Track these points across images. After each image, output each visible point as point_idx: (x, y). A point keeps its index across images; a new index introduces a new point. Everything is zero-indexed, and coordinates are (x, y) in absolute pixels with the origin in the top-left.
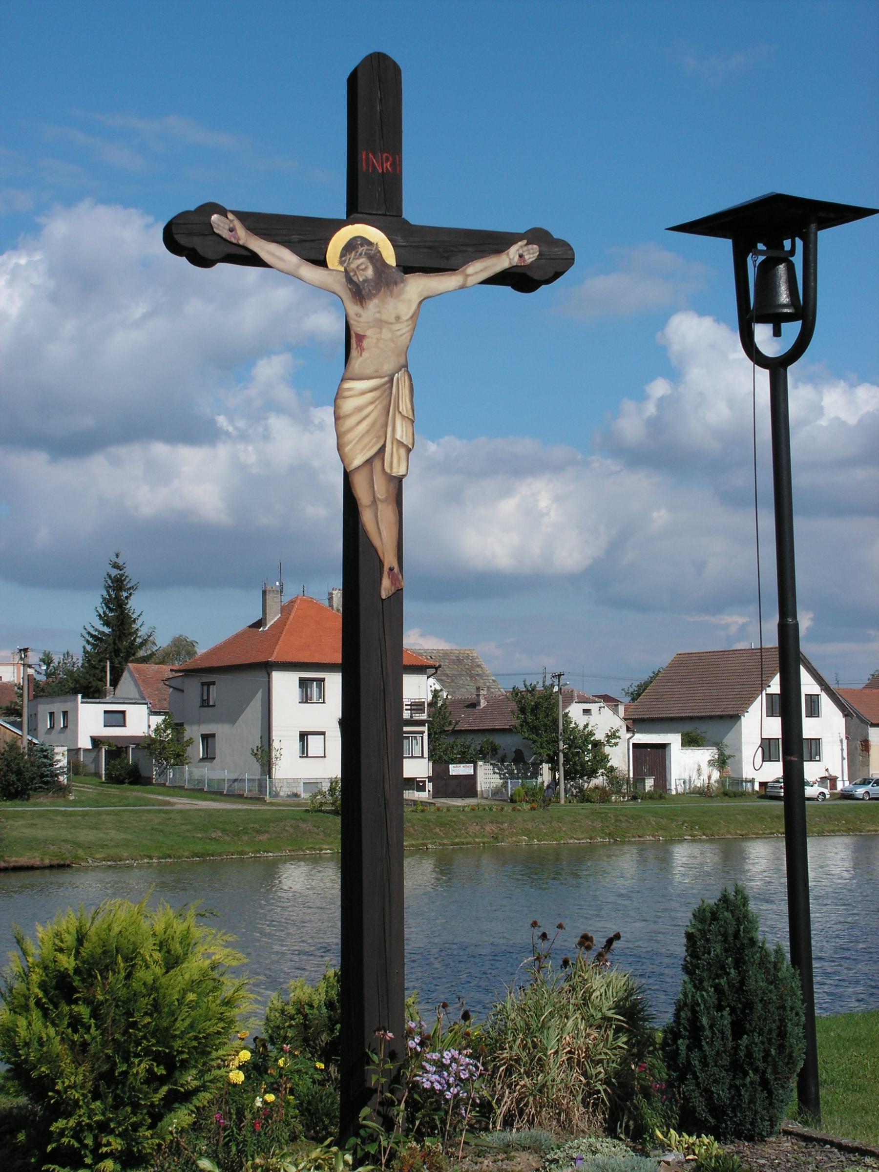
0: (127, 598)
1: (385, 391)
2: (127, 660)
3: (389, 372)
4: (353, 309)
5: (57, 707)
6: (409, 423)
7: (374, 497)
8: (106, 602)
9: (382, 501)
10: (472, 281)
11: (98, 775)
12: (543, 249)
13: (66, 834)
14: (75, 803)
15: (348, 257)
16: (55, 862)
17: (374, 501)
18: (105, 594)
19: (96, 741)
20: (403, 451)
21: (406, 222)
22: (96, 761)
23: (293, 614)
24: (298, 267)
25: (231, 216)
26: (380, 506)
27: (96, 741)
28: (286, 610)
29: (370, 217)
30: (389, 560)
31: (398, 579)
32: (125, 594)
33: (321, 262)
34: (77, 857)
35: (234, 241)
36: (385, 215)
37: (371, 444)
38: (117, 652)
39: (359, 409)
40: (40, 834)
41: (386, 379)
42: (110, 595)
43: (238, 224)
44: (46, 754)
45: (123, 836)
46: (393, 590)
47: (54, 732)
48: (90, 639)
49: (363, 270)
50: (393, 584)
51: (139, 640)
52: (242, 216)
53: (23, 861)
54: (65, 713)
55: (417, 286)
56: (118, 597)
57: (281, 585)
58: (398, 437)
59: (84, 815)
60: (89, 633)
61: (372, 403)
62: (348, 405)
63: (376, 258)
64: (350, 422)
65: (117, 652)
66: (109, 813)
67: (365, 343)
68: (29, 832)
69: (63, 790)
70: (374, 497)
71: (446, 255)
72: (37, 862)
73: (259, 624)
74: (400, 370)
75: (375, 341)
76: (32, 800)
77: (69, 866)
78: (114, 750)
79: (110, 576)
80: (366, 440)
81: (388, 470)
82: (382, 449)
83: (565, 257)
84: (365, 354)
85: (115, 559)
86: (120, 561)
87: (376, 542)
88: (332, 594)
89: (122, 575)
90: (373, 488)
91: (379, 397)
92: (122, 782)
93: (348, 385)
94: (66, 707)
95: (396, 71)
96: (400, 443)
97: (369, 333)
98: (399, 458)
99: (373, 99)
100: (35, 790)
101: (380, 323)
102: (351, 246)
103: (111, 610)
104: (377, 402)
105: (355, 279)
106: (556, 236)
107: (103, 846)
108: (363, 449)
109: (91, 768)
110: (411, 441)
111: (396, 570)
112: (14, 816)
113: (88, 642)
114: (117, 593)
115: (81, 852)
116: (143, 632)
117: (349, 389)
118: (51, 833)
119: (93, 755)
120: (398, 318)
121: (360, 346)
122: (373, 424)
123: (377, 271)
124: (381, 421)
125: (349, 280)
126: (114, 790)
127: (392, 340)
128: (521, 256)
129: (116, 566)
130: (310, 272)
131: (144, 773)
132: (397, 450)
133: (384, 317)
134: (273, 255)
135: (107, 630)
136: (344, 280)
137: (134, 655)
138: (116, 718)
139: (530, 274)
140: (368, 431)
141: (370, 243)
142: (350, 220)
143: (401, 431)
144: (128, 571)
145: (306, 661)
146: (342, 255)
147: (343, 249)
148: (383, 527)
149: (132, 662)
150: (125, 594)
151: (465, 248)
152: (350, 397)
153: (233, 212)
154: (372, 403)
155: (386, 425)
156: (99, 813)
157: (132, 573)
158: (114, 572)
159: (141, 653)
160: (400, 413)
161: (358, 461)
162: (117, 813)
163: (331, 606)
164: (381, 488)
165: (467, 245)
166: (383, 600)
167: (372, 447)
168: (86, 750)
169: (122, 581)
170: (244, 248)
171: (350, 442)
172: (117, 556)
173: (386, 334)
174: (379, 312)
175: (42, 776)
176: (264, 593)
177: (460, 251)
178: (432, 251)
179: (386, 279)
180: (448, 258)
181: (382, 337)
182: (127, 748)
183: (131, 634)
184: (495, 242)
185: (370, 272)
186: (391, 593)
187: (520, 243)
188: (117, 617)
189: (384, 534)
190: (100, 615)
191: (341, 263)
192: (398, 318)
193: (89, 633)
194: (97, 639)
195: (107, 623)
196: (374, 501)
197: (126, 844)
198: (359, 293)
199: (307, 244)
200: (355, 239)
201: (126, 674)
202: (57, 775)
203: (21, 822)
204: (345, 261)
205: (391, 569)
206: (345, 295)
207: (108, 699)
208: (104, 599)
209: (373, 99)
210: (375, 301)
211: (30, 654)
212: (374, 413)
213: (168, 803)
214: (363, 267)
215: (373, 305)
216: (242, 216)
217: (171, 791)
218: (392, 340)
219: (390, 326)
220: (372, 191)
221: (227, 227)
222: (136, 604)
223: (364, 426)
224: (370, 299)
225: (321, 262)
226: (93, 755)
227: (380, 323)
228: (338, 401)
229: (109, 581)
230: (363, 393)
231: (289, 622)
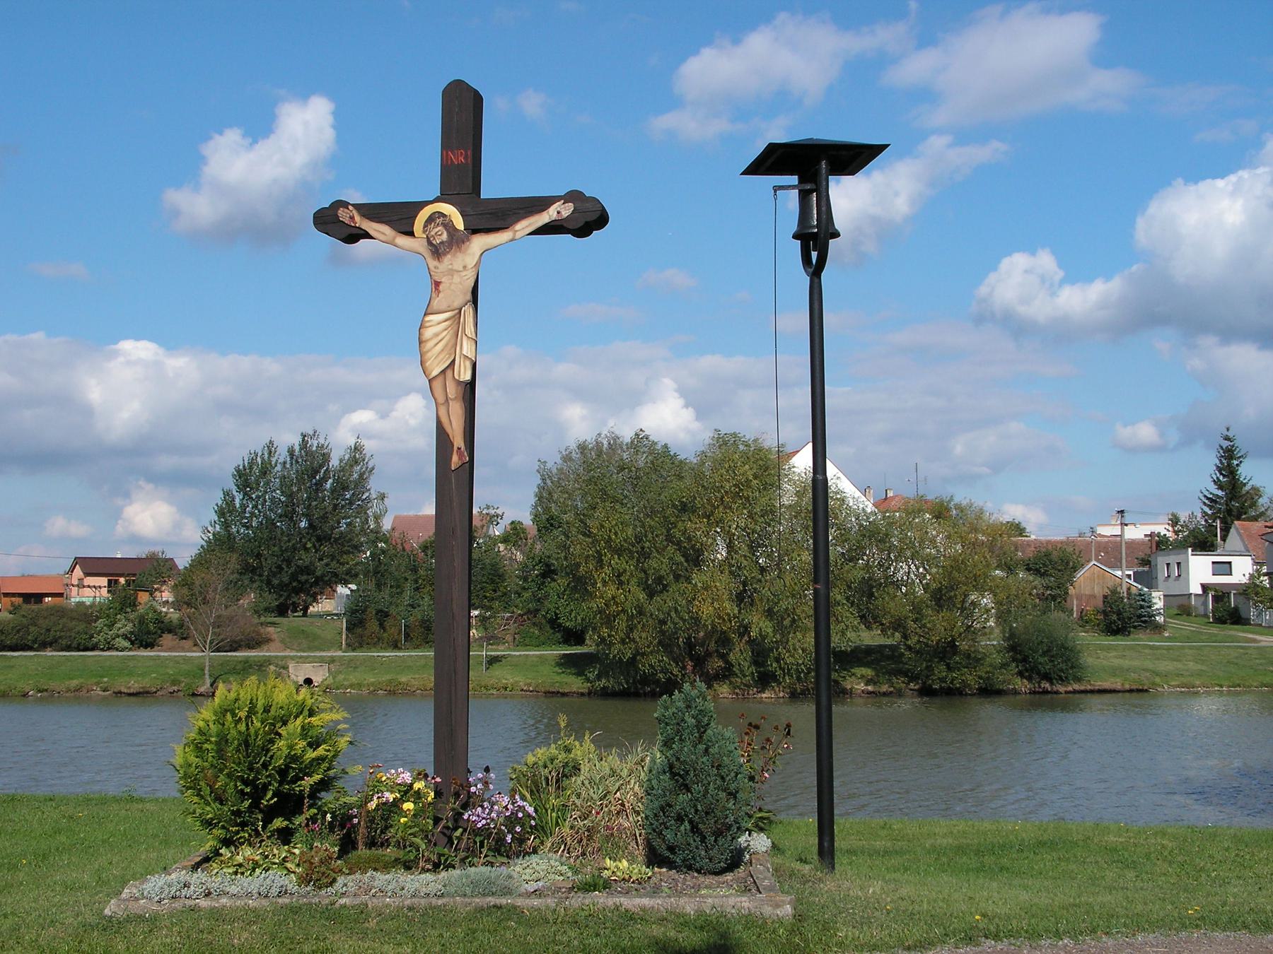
4: (432, 263)
5: (1173, 559)
8: (1220, 470)
10: (518, 235)
11: (1206, 616)
13: (1149, 664)
14: (1169, 639)
16: (1134, 687)
19: (1205, 587)
22: (1205, 604)
27: (1205, 587)
32: (1235, 462)
33: (411, 234)
34: (1154, 684)
39: (437, 335)
40: (1126, 663)
43: (355, 212)
44: (1146, 601)
45: (1200, 667)
47: (1171, 580)
52: (358, 207)
53: (1106, 685)
54: (1179, 564)
55: (479, 243)
56: (1229, 465)
59: (1169, 648)
62: (428, 333)
63: (449, 226)
64: (429, 345)
65: (1229, 512)
66: (1190, 648)
67: (441, 288)
68: (1117, 662)
69: (1158, 628)
72: (1119, 687)
76: (1132, 636)
77: (1146, 691)
78: (1219, 594)
82: (454, 361)
86: (1230, 434)
92: (1224, 622)
93: (427, 318)
94: (1179, 558)
99: (463, 113)
100: (1135, 627)
101: (451, 272)
102: (431, 219)
107: (1178, 675)
109: (1201, 610)
112: (1109, 648)
115: (1158, 680)
118: (1136, 663)
119: (1202, 599)
120: (465, 267)
122: (446, 345)
123: (449, 234)
125: (430, 243)
126: (1215, 630)
129: (1227, 438)
130: (403, 241)
131: (1243, 615)
133: (455, 267)
135: (1220, 493)
138: (1223, 568)
141: (444, 216)
142: (437, 200)
143: (467, 348)
146: (425, 226)
150: (1235, 462)
153: (353, 205)
156: (1183, 647)
157: (1241, 444)
158: (1226, 444)
161: (435, 373)
162: (1199, 648)
164: (452, 390)
168: (1196, 595)
173: (456, 279)
175: (1140, 616)
178: (493, 217)
179: (456, 241)
182: (1229, 594)
184: (540, 204)
185: (445, 237)
192: (465, 267)
194: (1213, 501)
195: (1221, 488)
197: (1200, 674)
198: (437, 251)
201: (1232, 530)
202: (1154, 616)
203: (1114, 654)
206: (427, 254)
207: (1219, 551)
209: (463, 113)
212: (447, 336)
213: (1255, 641)
215: (447, 259)
217: (1266, 631)
220: (461, 179)
225: (411, 234)
226: (1202, 599)
227: (451, 272)
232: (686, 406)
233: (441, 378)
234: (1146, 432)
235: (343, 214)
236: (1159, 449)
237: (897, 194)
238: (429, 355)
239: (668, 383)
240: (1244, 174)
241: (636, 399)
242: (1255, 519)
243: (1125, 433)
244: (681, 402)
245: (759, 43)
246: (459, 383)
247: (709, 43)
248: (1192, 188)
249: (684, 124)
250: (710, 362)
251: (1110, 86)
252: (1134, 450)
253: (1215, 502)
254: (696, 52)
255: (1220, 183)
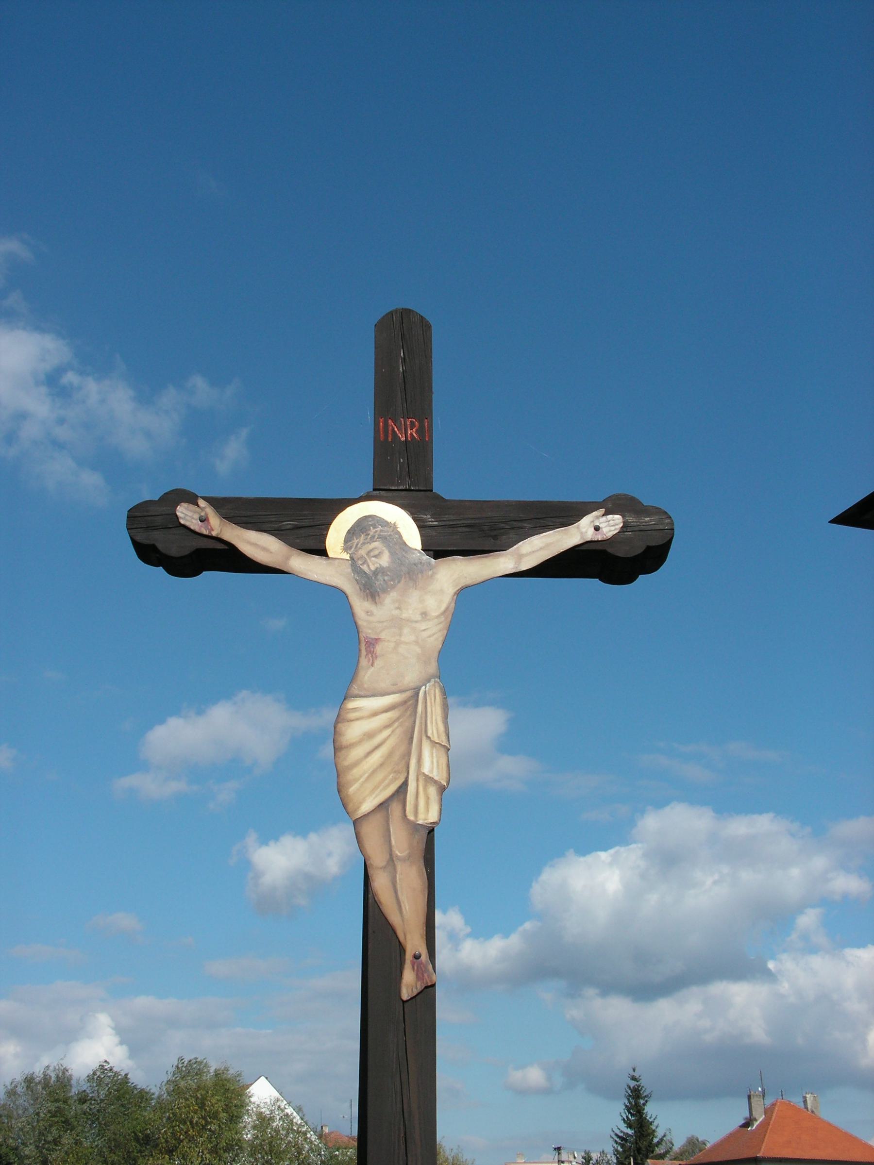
0: (644, 1104)
1: (406, 710)
2: (647, 1157)
3: (412, 685)
6: (442, 752)
7: (391, 855)
8: (628, 1109)
9: (403, 860)
12: (630, 519)
15: (356, 541)
17: (391, 860)
18: (627, 1102)
20: (433, 791)
21: (438, 497)
23: (774, 1115)
24: (288, 558)
25: (202, 503)
26: (399, 867)
28: (768, 1111)
29: (390, 494)
30: (414, 943)
31: (427, 970)
33: (322, 552)
35: (205, 532)
36: (410, 490)
37: (387, 782)
38: (639, 1150)
39: (370, 735)
41: (409, 694)
42: (630, 1102)
43: (210, 512)
46: (420, 987)
48: (618, 1140)
49: (375, 556)
50: (419, 976)
51: (655, 1140)
57: (763, 1090)
58: (426, 770)
60: (616, 1135)
61: (387, 727)
63: (391, 537)
64: (356, 753)
65: (639, 1150)
67: (378, 649)
70: (391, 855)
71: (495, 533)
73: (747, 1124)
74: (429, 681)
75: (392, 645)
79: (629, 1087)
80: (379, 776)
81: (411, 817)
82: (405, 784)
83: (661, 527)
84: (378, 663)
85: (632, 1073)
86: (636, 1075)
87: (394, 918)
88: (805, 1097)
89: (639, 1086)
90: (390, 841)
91: (398, 719)
95: (425, 326)
96: (429, 780)
97: (383, 636)
98: (428, 799)
99: (404, 360)
103: (632, 1115)
104: (396, 725)
105: (365, 568)
106: (646, 502)
108: (376, 788)
110: (445, 775)
111: (424, 957)
113: (616, 1142)
114: (636, 1100)
116: (659, 1133)
117: (355, 710)
121: (372, 653)
122: (390, 754)
124: (403, 748)
127: (416, 642)
128: (597, 529)
129: (633, 1078)
132: (425, 789)
134: (255, 545)
135: (630, 1131)
136: (350, 570)
137: (653, 1152)
139: (610, 550)
140: (382, 765)
142: (368, 498)
144: (643, 1083)
145: (788, 1156)
147: (349, 532)
148: (403, 898)
149: (652, 1158)
150: (642, 1102)
151: (520, 524)
152: (357, 719)
154: (387, 727)
155: (408, 754)
158: (633, 1084)
159: (659, 1150)
160: (428, 738)
161: (367, 806)
163: (806, 1108)
164: (402, 842)
165: (522, 521)
166: (404, 1002)
167: (388, 785)
169: (639, 1091)
170: (218, 539)
171: (356, 780)
172: (634, 1070)
174: (399, 608)
176: (749, 1097)
177: (513, 528)
180: (495, 537)
181: (403, 639)
183: (649, 1135)
186: (415, 992)
187: (595, 513)
188: (638, 1120)
189: (406, 906)
190: (624, 1119)
191: (346, 549)
193: (616, 1135)
195: (630, 1126)
196: (391, 860)
199: (302, 531)
200: (366, 518)
204: (351, 548)
205: (417, 957)
208: (626, 1106)
209: (404, 360)
210: (394, 595)
211: (562, 1151)
212: (391, 739)
214: (376, 552)
215: (389, 600)
216: (217, 503)
218: (416, 642)
219: (414, 625)
221: (197, 516)
222: (651, 1110)
223: (376, 757)
224: (385, 591)
228: (340, 725)
229: (629, 1091)
230: (375, 714)
231: (772, 1122)
232: (121, 1043)
233: (378, 818)
234: (535, 1075)
235: (186, 514)
236: (546, 1091)
237: (330, 854)
238: (356, 772)
239: (103, 1020)
240: (622, 849)
241: (71, 1035)
242: (661, 1157)
243: (516, 1076)
244: (116, 1039)
245: (220, 715)
246: (414, 827)
247: (176, 712)
248: (582, 859)
249: (149, 785)
250: (143, 1002)
251: (513, 768)
252: (523, 1092)
253: (626, 1140)
254: (162, 722)
255: (603, 856)
